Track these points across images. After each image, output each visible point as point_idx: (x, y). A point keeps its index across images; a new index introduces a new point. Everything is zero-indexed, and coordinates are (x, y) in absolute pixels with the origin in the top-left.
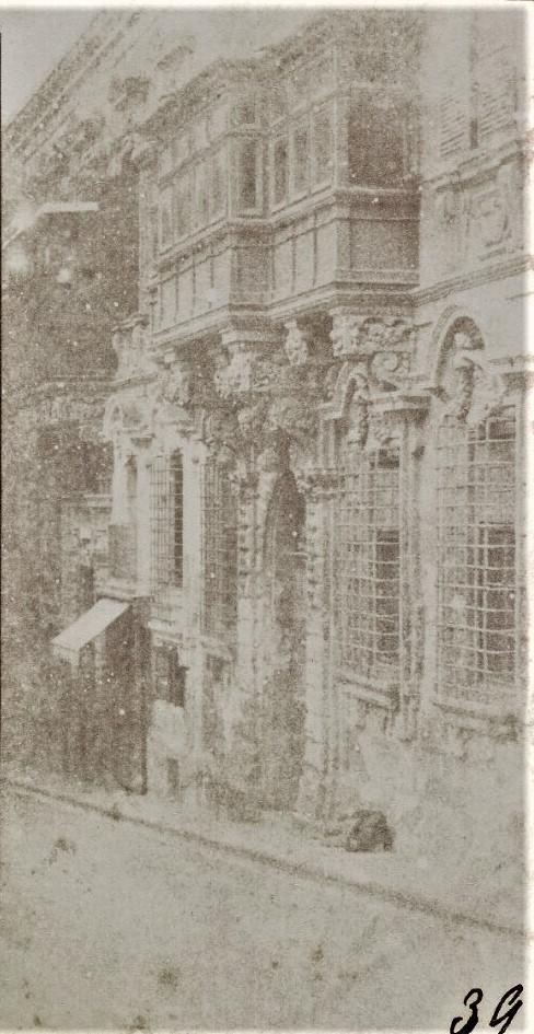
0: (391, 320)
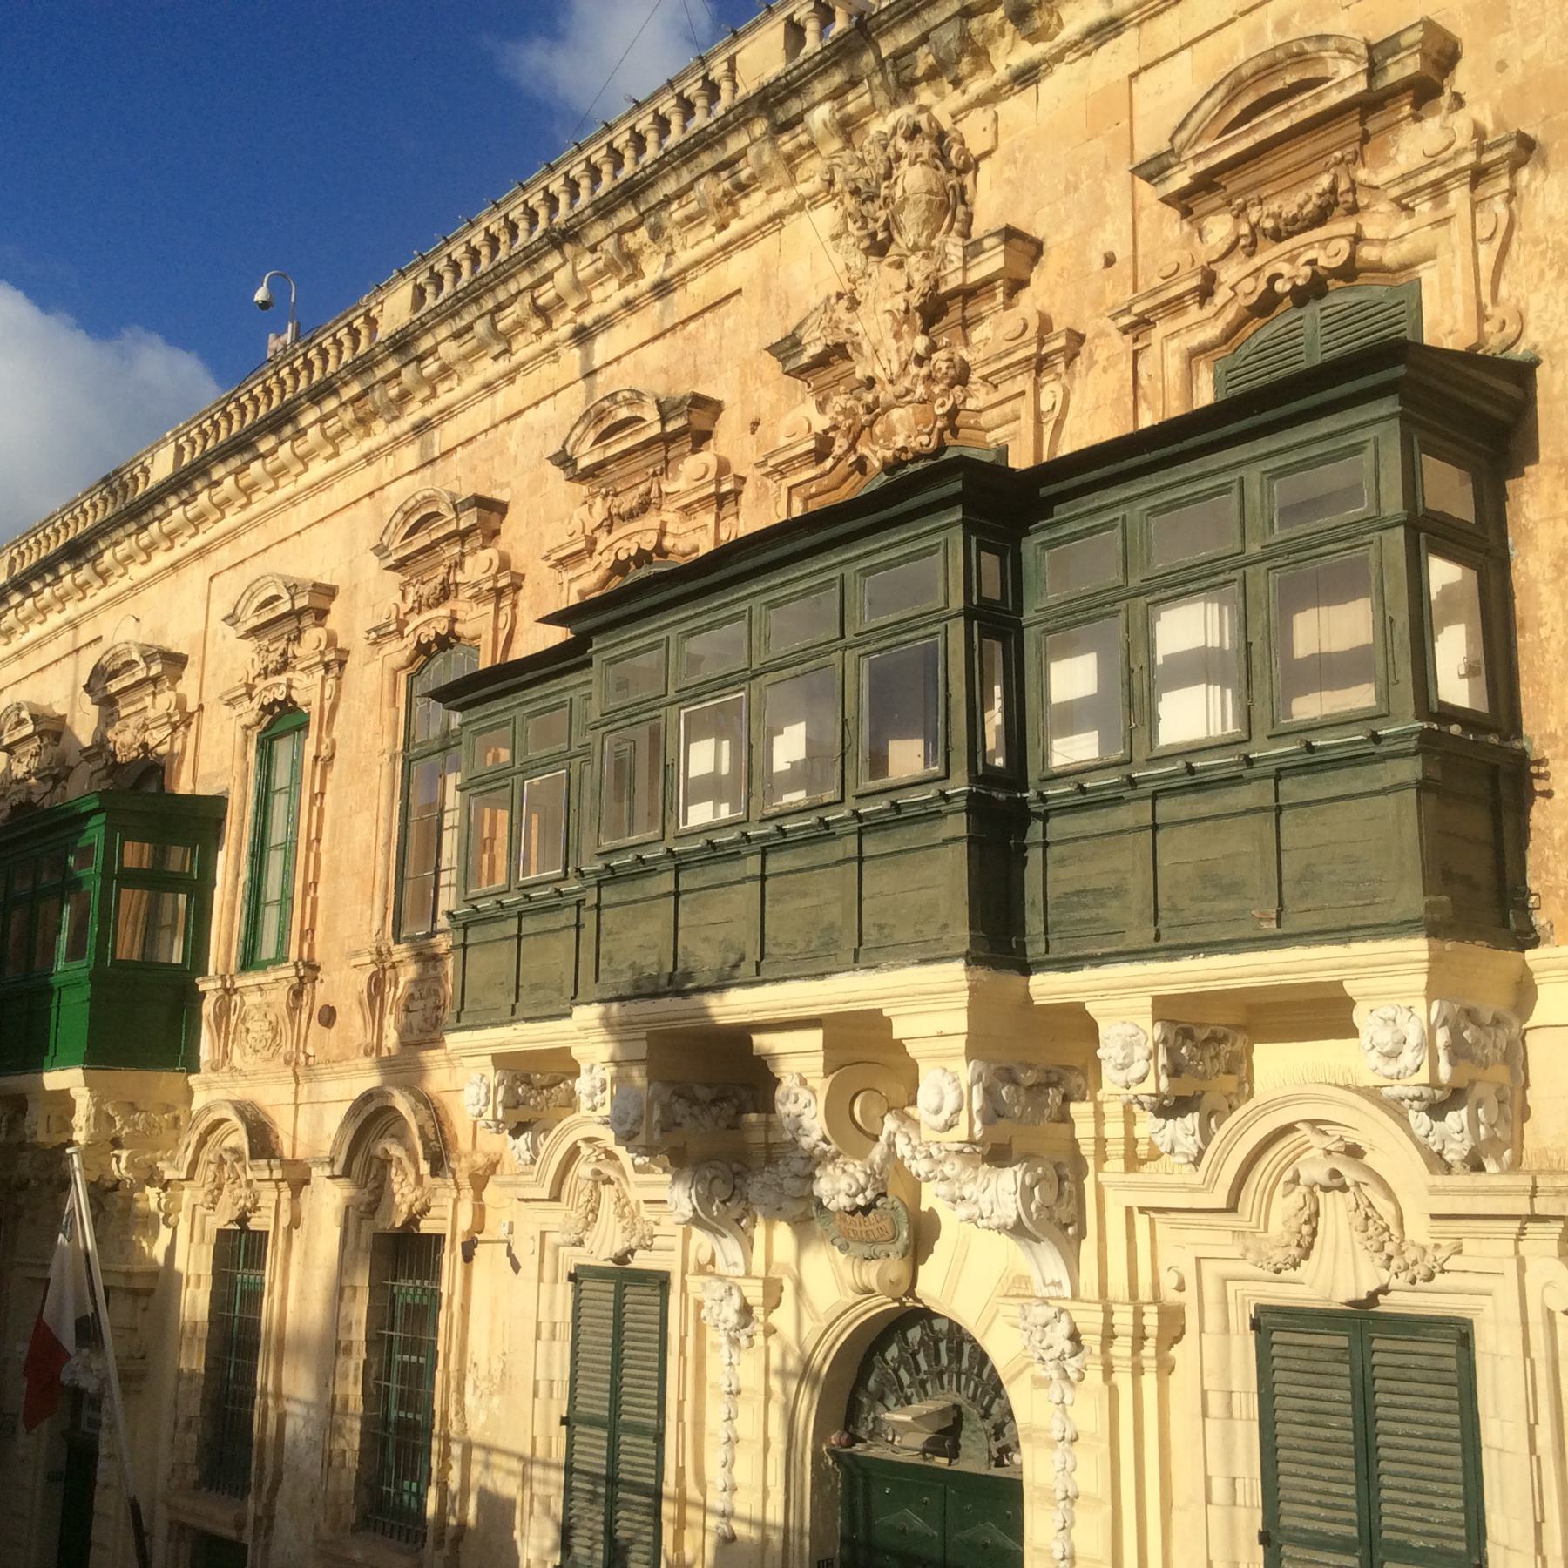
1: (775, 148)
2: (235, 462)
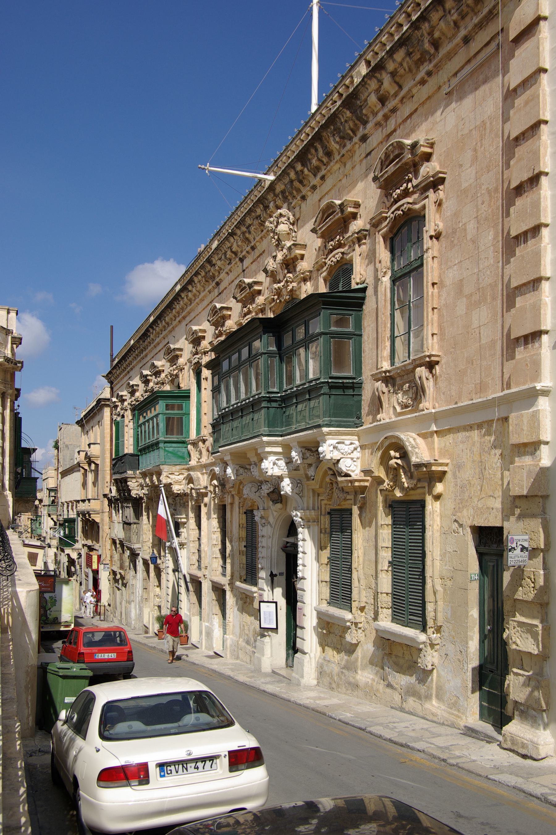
0: (348, 442)
1: (266, 212)
2: (185, 293)
